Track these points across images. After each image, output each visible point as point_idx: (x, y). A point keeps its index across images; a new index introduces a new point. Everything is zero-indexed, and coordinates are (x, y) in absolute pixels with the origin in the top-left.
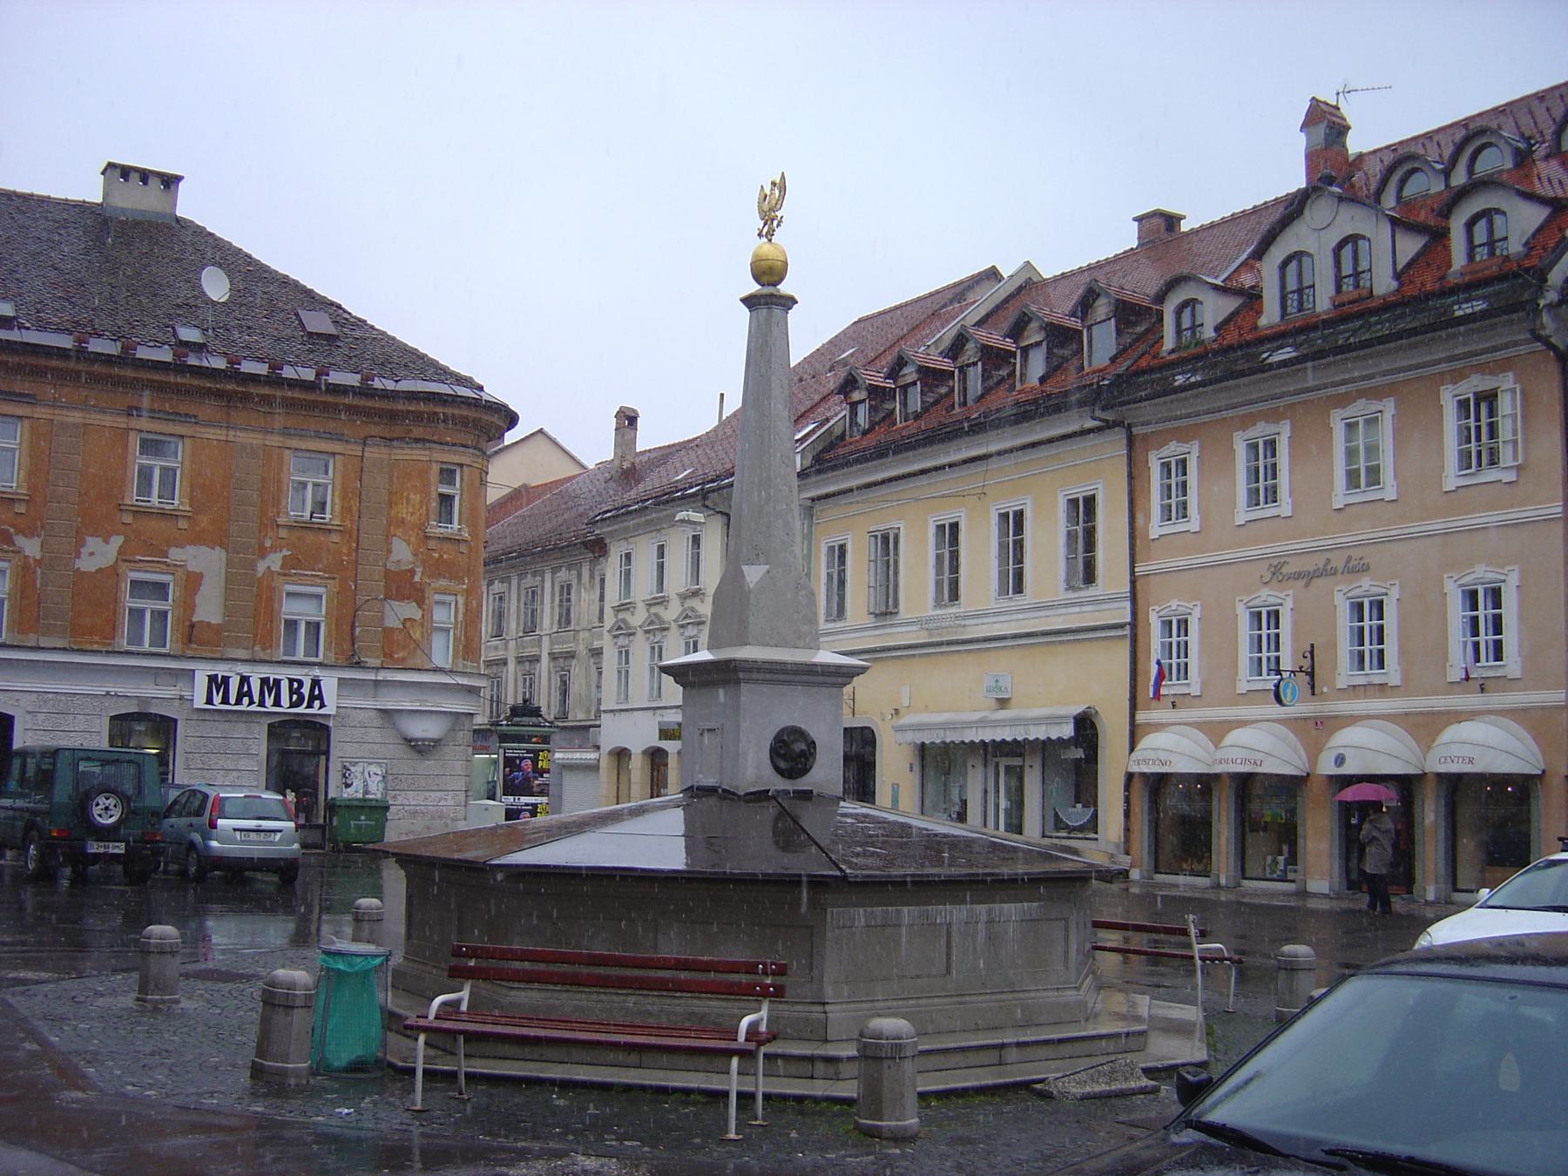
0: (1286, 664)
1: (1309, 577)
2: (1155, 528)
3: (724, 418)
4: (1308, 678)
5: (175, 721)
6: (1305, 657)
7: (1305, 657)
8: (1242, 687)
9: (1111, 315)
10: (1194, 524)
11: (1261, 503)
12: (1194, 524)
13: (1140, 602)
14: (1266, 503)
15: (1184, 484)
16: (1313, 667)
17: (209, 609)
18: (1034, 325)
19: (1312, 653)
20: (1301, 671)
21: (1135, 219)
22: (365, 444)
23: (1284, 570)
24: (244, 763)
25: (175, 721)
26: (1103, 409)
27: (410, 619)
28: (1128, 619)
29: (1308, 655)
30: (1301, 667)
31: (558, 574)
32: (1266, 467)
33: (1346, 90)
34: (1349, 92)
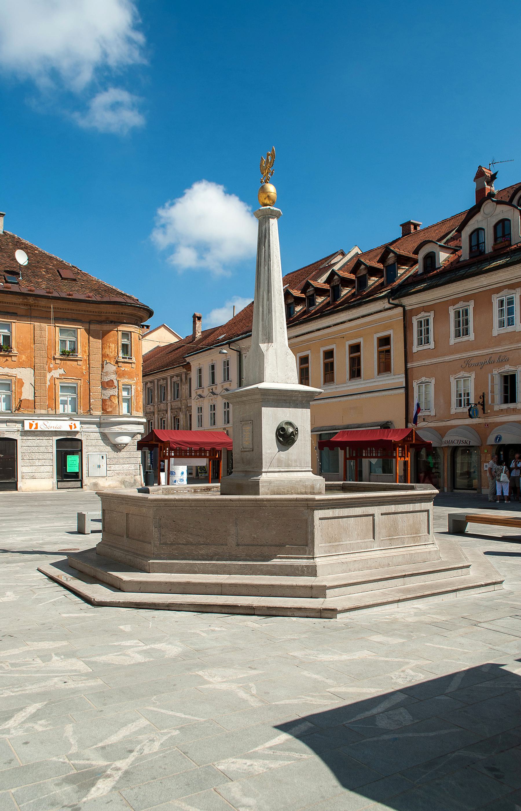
0: (472, 401)
1: (482, 365)
2: (415, 348)
3: (235, 316)
4: (482, 407)
5: (16, 440)
6: (481, 398)
7: (481, 398)
8: (453, 411)
9: (396, 261)
10: (432, 345)
11: (423, 344)
12: (432, 345)
13: (409, 378)
14: (463, 336)
15: (428, 329)
16: (483, 401)
17: (27, 394)
18: (363, 267)
19: (483, 396)
20: (479, 404)
21: (401, 225)
22: (236, 524)
23: (472, 362)
24: (47, 456)
25: (16, 440)
26: (393, 300)
27: (113, 395)
28: (404, 385)
29: (482, 397)
30: (479, 402)
31: (173, 379)
32: (463, 320)
33: (493, 162)
34: (495, 163)
